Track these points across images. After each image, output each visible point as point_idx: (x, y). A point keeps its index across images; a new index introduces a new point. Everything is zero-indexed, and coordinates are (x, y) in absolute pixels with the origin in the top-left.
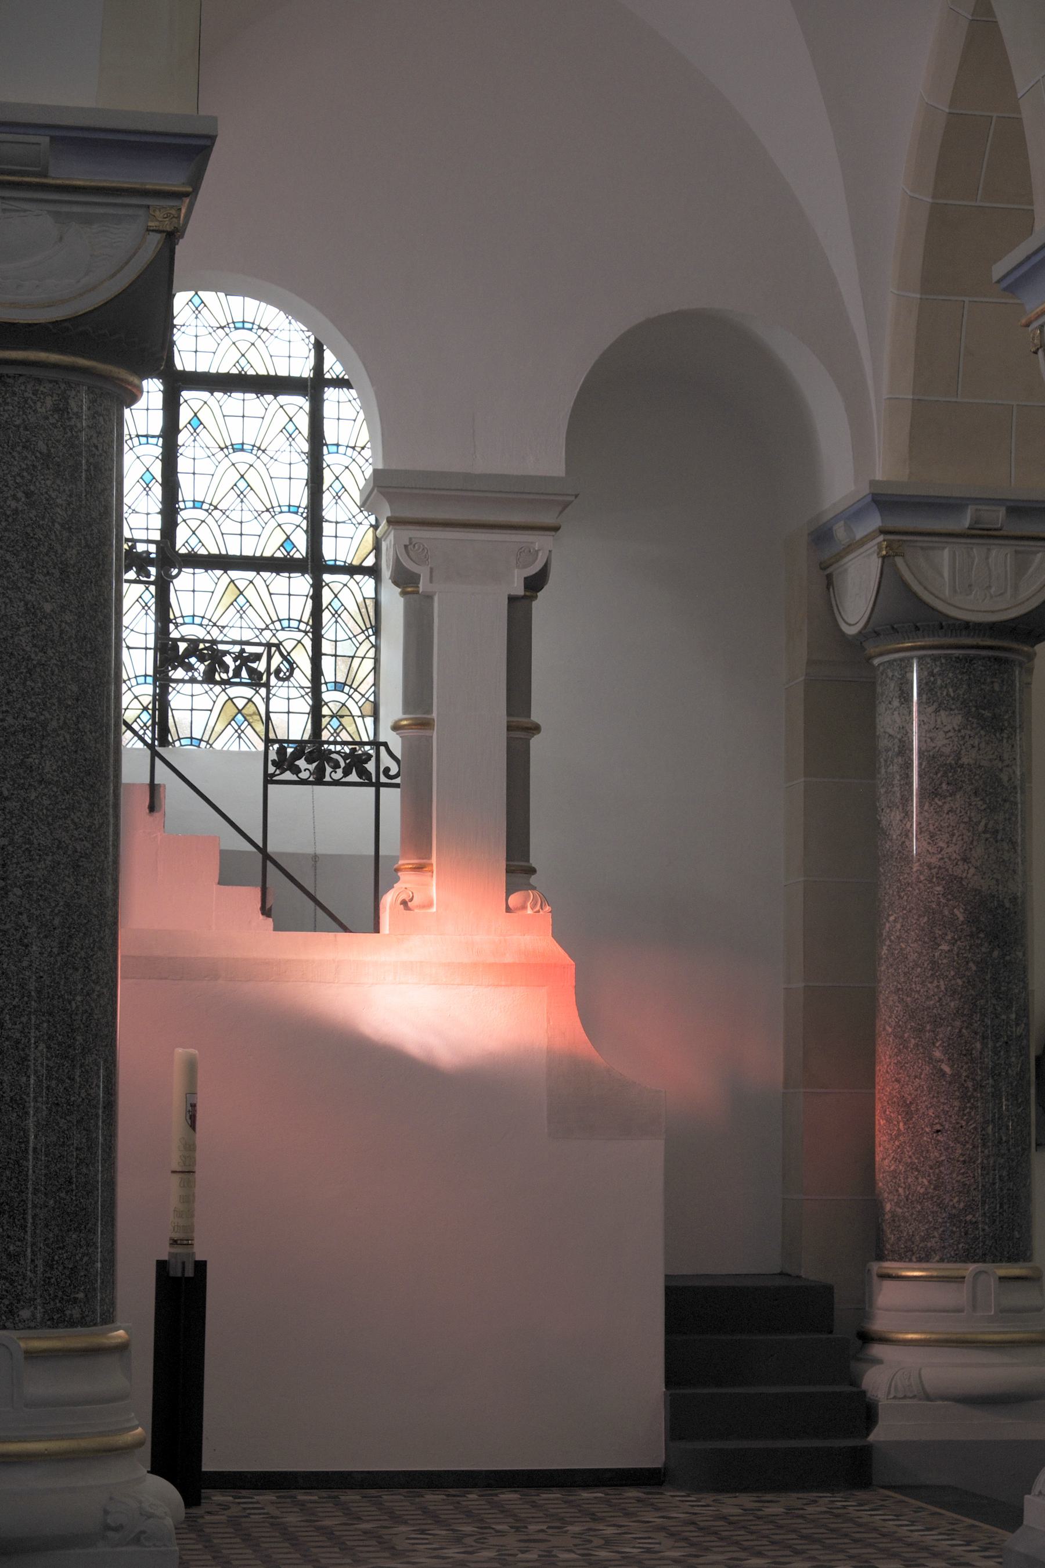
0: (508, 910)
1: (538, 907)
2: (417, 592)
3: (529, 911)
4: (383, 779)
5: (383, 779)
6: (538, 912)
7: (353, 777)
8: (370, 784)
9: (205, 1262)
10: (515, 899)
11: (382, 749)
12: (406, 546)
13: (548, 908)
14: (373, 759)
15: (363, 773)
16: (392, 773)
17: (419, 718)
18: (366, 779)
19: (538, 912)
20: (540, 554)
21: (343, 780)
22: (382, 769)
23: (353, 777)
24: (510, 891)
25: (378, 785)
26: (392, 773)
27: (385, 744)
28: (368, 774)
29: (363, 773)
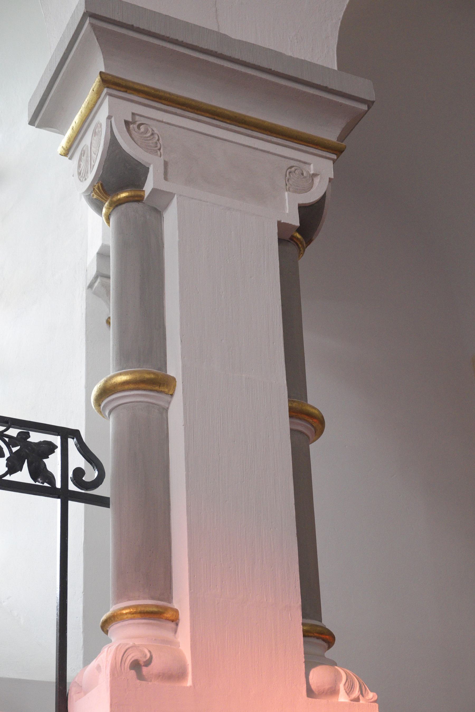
0: (310, 693)
1: (356, 693)
2: (138, 199)
3: (343, 698)
4: (72, 487)
5: (72, 487)
6: (357, 700)
7: (23, 476)
8: (51, 492)
9: (299, 205)
10: (319, 676)
11: (71, 443)
12: (127, 123)
13: (371, 695)
14: (58, 451)
15: (39, 471)
16: (87, 478)
17: (141, 377)
18: (42, 485)
19: (357, 700)
20: (317, 181)
21: (8, 478)
22: (70, 474)
23: (23, 476)
24: (311, 662)
25: (65, 496)
26: (87, 478)
27: (75, 434)
28: (50, 478)
29: (39, 471)
